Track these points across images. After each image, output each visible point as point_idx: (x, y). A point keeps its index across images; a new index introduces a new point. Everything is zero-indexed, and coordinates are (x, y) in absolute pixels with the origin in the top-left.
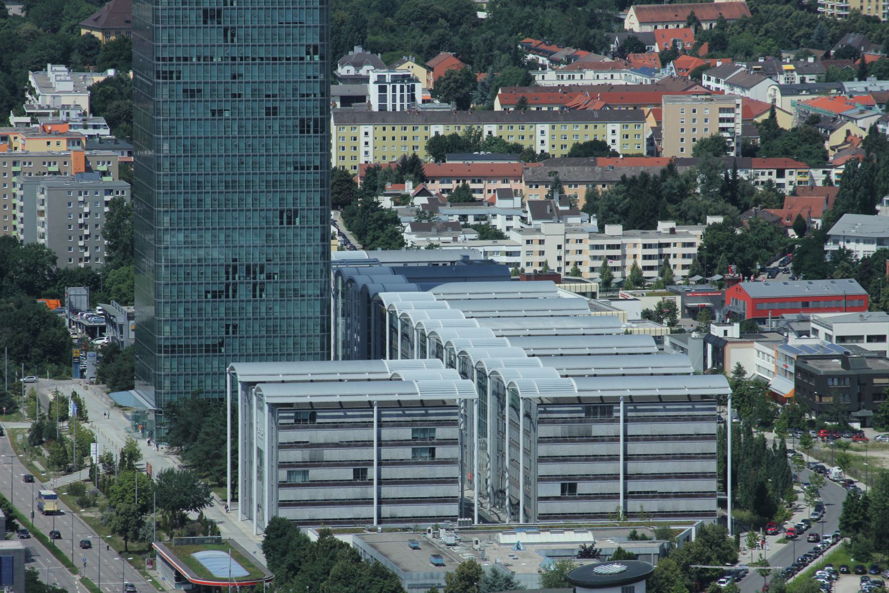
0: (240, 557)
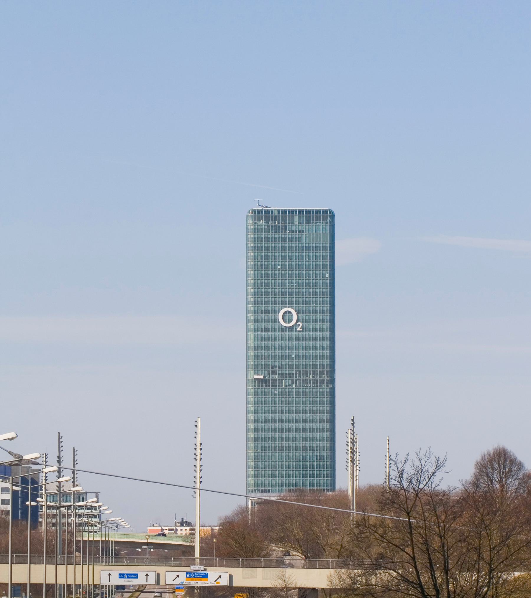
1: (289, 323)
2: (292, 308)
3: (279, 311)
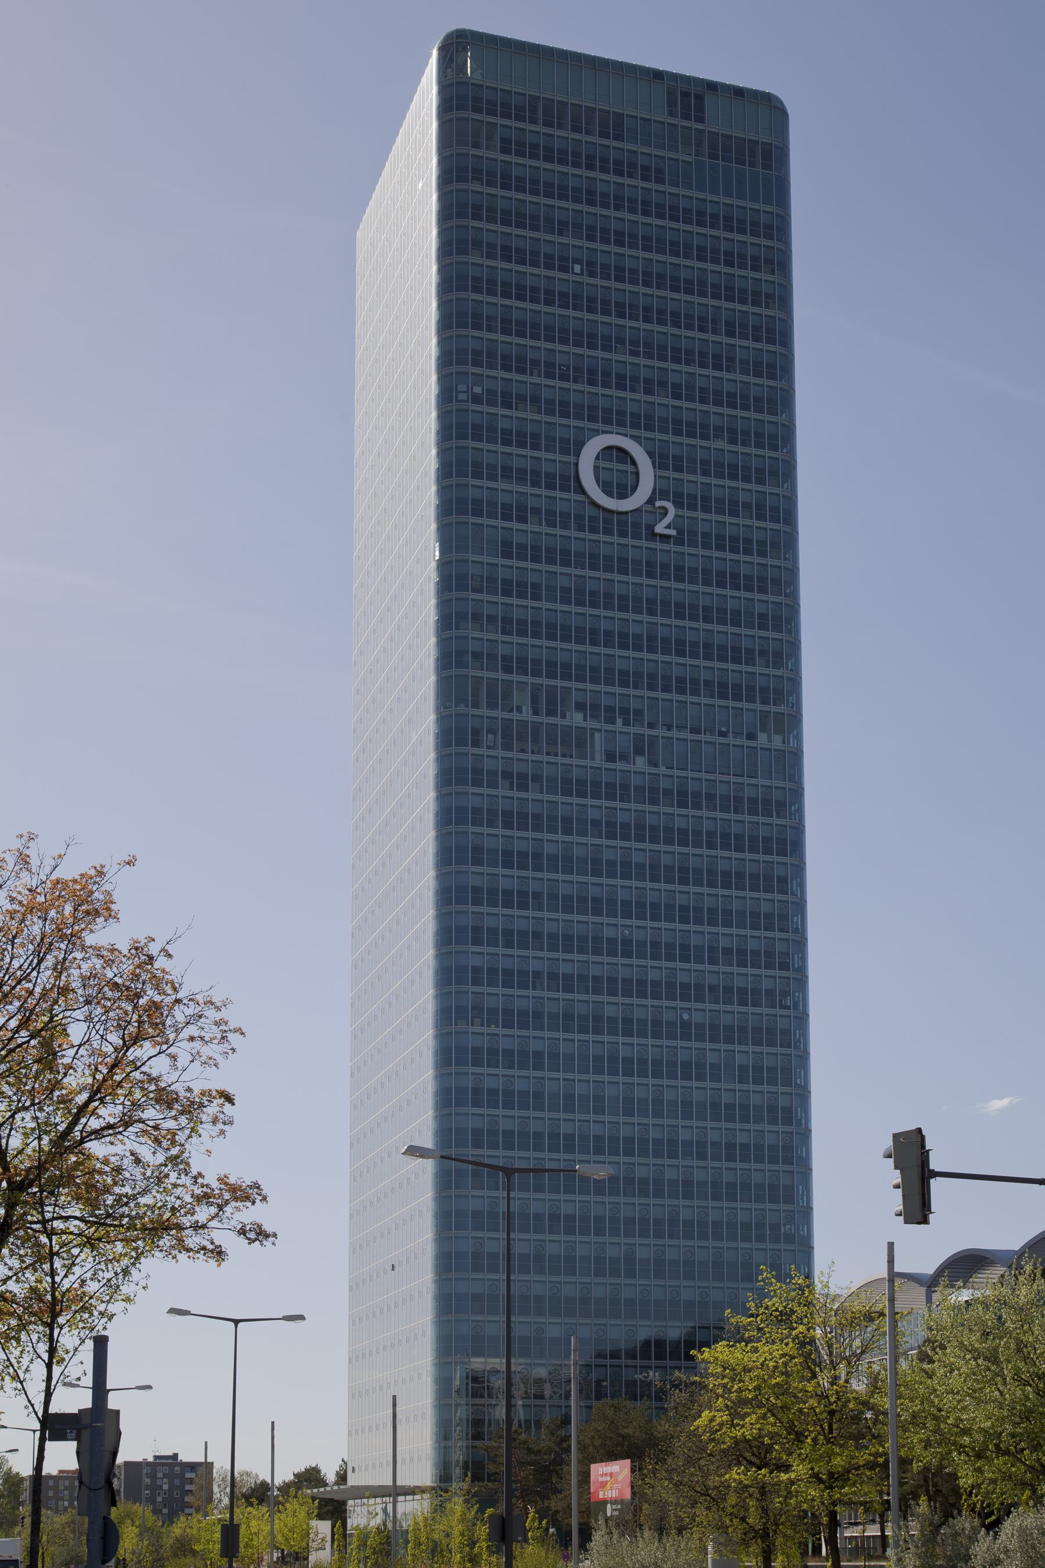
0: (97, 1134)
1: (623, 496)
2: (636, 439)
3: (580, 445)
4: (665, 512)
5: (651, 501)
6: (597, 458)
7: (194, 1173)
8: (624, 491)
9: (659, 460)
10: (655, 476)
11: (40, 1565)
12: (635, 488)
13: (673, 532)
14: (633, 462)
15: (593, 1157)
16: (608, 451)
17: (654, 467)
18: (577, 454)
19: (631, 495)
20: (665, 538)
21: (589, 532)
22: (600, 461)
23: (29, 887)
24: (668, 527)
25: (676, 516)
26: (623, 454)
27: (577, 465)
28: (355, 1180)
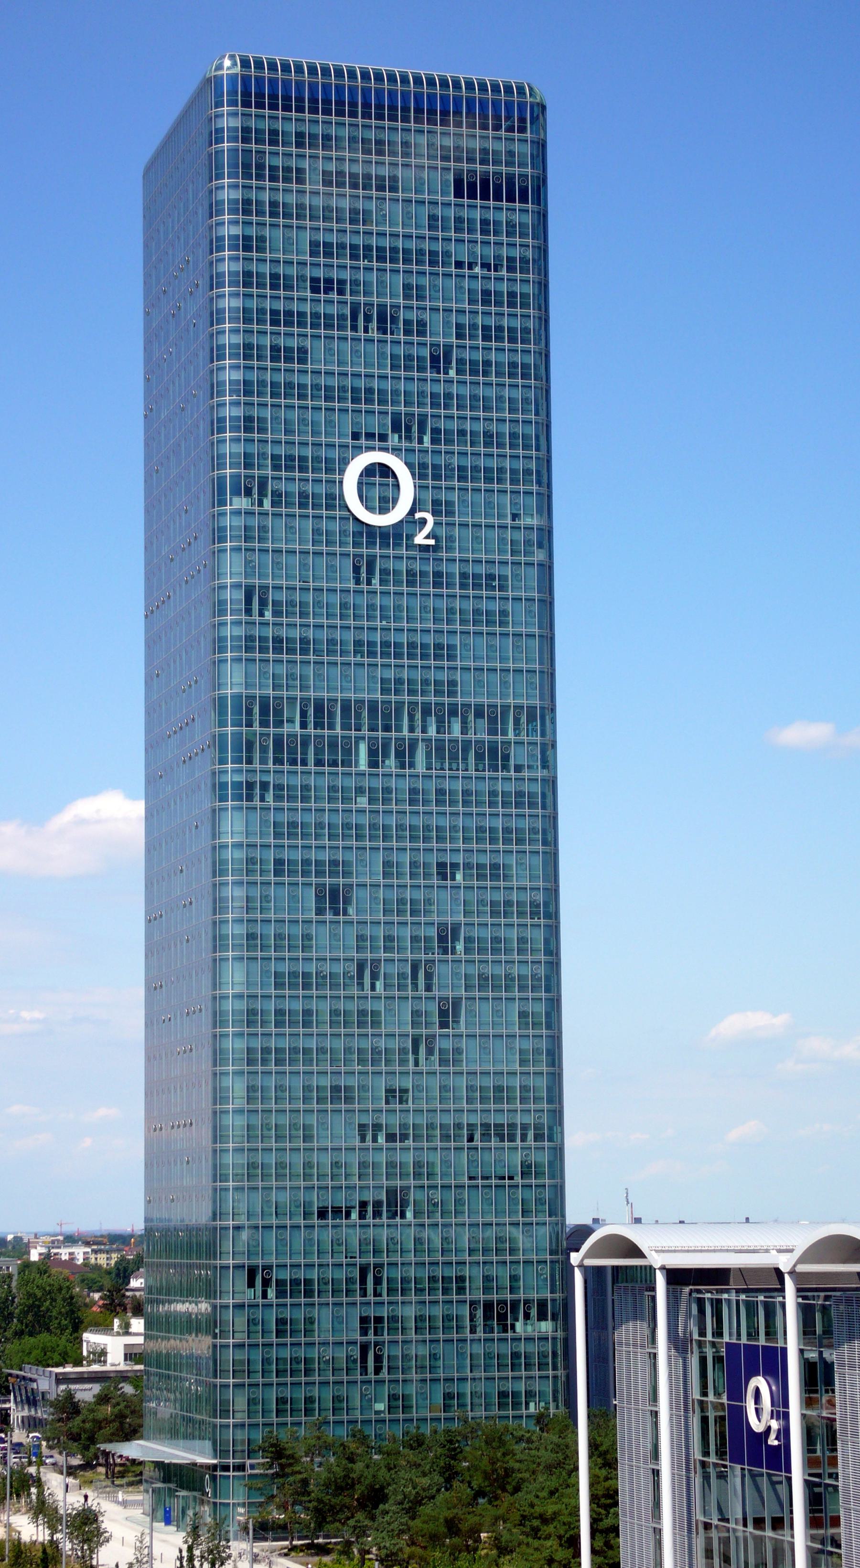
1: (384, 510)
4: (424, 522)
5: (412, 512)
6: (361, 475)
7: (443, 1529)
8: (385, 506)
9: (419, 472)
10: (415, 486)
11: (2, 1259)
12: (395, 501)
13: (432, 542)
14: (395, 476)
15: (234, 1045)
16: (370, 471)
17: (414, 478)
18: (342, 472)
19: (393, 508)
20: (425, 548)
21: (380, 477)
22: (364, 478)
23: (550, 1426)
24: (427, 537)
25: (435, 523)
26: (385, 471)
27: (341, 482)
28: (149, 1132)
